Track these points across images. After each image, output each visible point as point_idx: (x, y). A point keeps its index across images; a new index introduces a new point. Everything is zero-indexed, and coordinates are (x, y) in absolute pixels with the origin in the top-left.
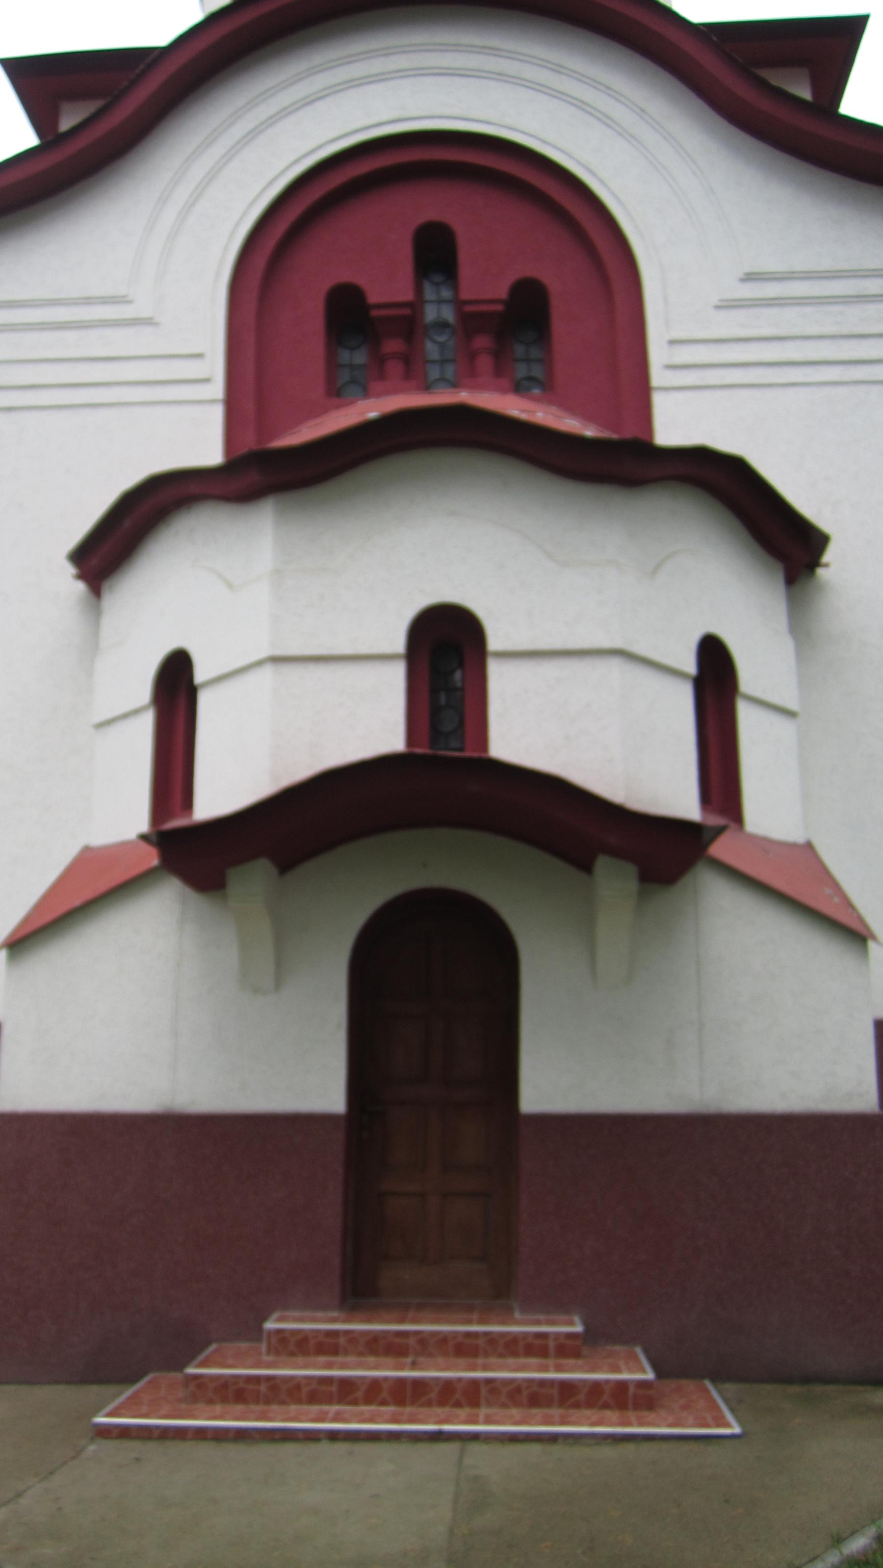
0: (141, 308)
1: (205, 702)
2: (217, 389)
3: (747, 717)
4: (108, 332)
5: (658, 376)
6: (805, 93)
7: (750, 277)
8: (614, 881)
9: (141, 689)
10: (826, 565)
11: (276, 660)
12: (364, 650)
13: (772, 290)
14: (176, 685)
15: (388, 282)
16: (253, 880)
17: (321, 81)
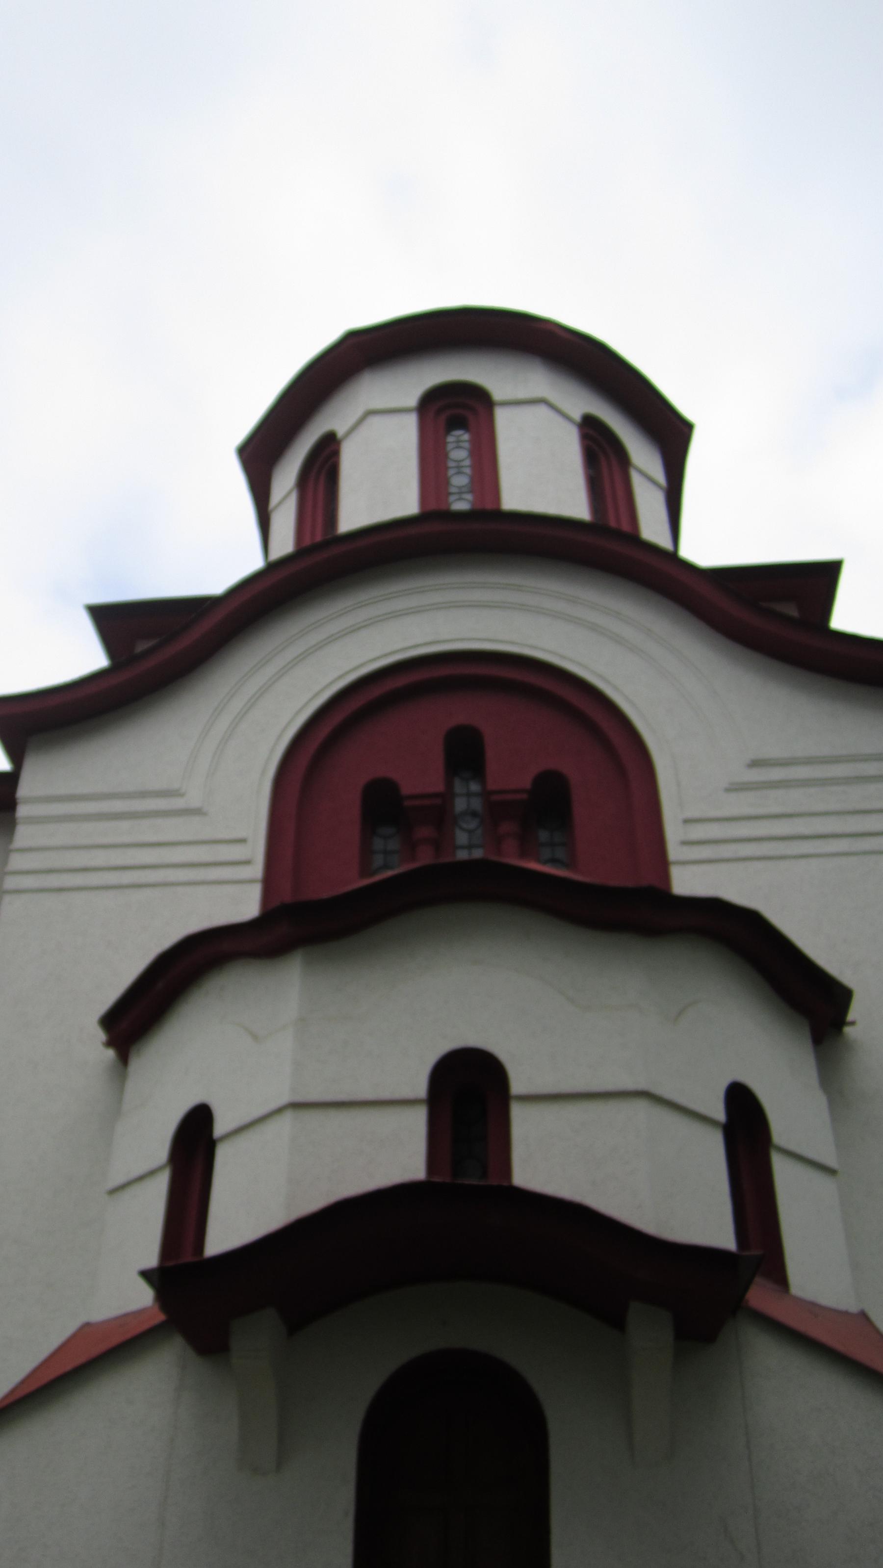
0: (194, 799)
1: (225, 1159)
2: (257, 870)
3: (782, 1171)
4: (159, 821)
5: (674, 851)
6: (792, 611)
7: (755, 764)
8: (649, 1334)
9: (156, 1147)
10: (853, 1023)
11: (296, 1106)
12: (386, 1095)
13: (776, 774)
14: (195, 1142)
15: (419, 775)
16: (257, 1337)
17: (363, 615)
